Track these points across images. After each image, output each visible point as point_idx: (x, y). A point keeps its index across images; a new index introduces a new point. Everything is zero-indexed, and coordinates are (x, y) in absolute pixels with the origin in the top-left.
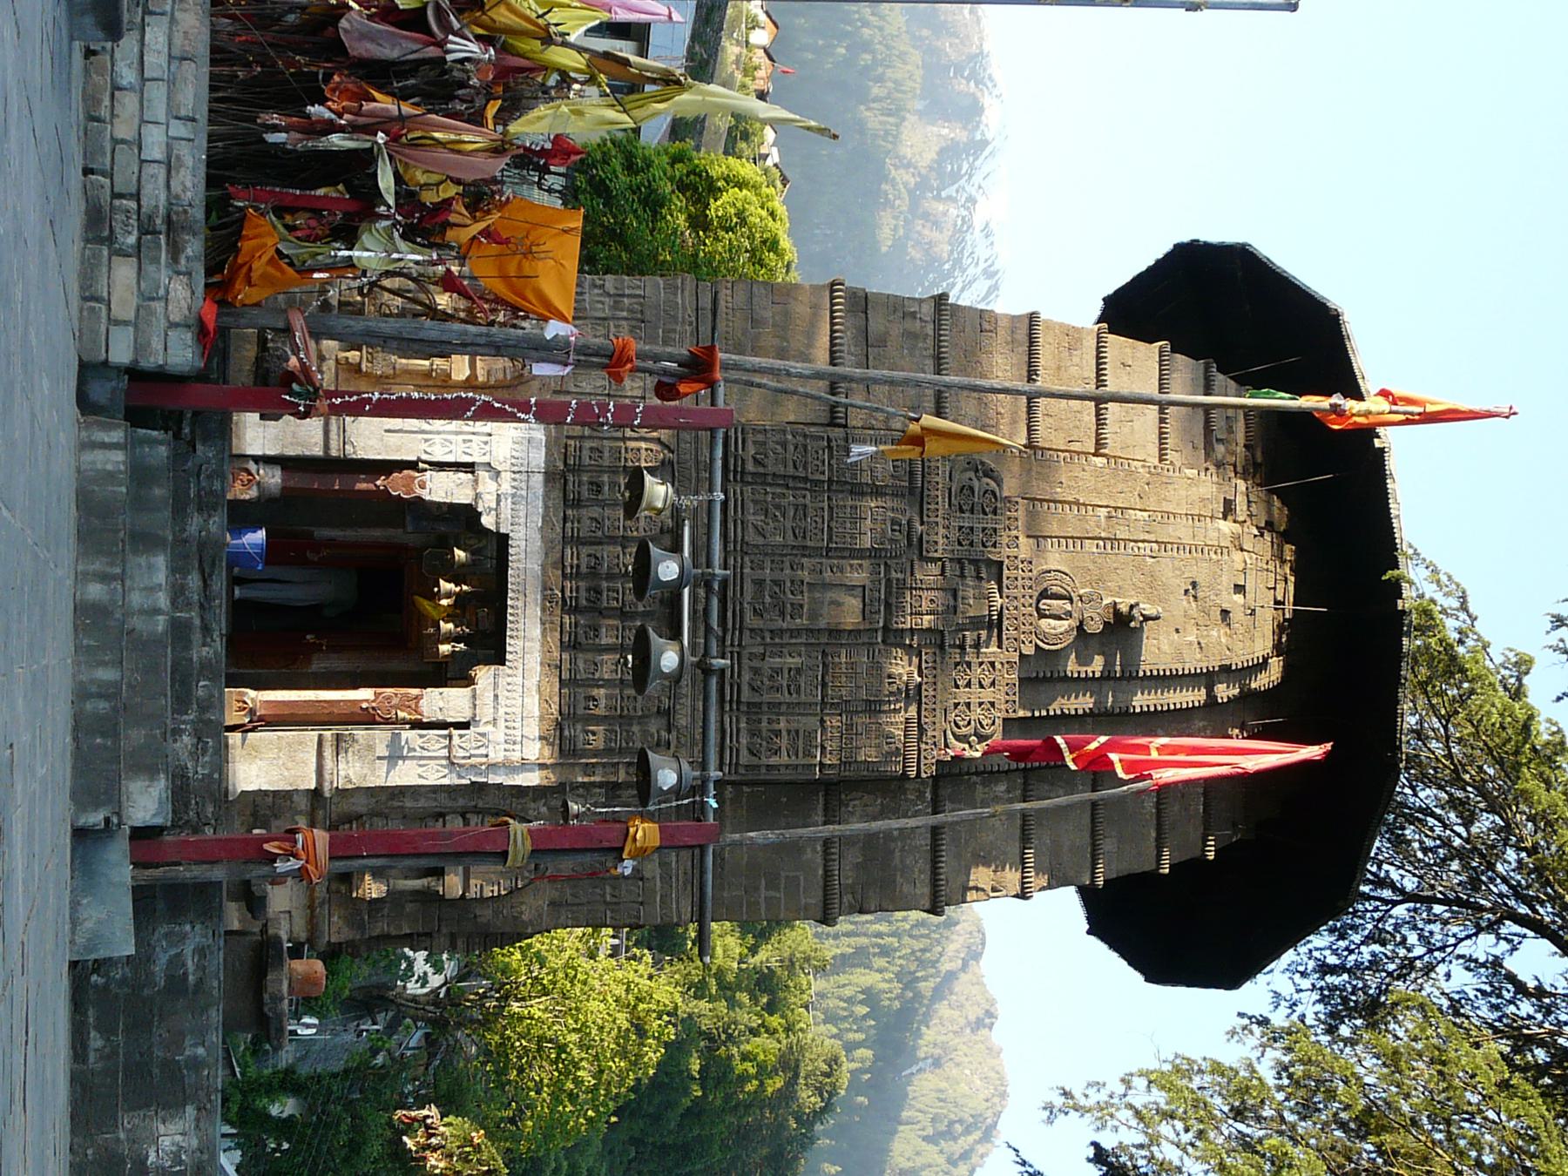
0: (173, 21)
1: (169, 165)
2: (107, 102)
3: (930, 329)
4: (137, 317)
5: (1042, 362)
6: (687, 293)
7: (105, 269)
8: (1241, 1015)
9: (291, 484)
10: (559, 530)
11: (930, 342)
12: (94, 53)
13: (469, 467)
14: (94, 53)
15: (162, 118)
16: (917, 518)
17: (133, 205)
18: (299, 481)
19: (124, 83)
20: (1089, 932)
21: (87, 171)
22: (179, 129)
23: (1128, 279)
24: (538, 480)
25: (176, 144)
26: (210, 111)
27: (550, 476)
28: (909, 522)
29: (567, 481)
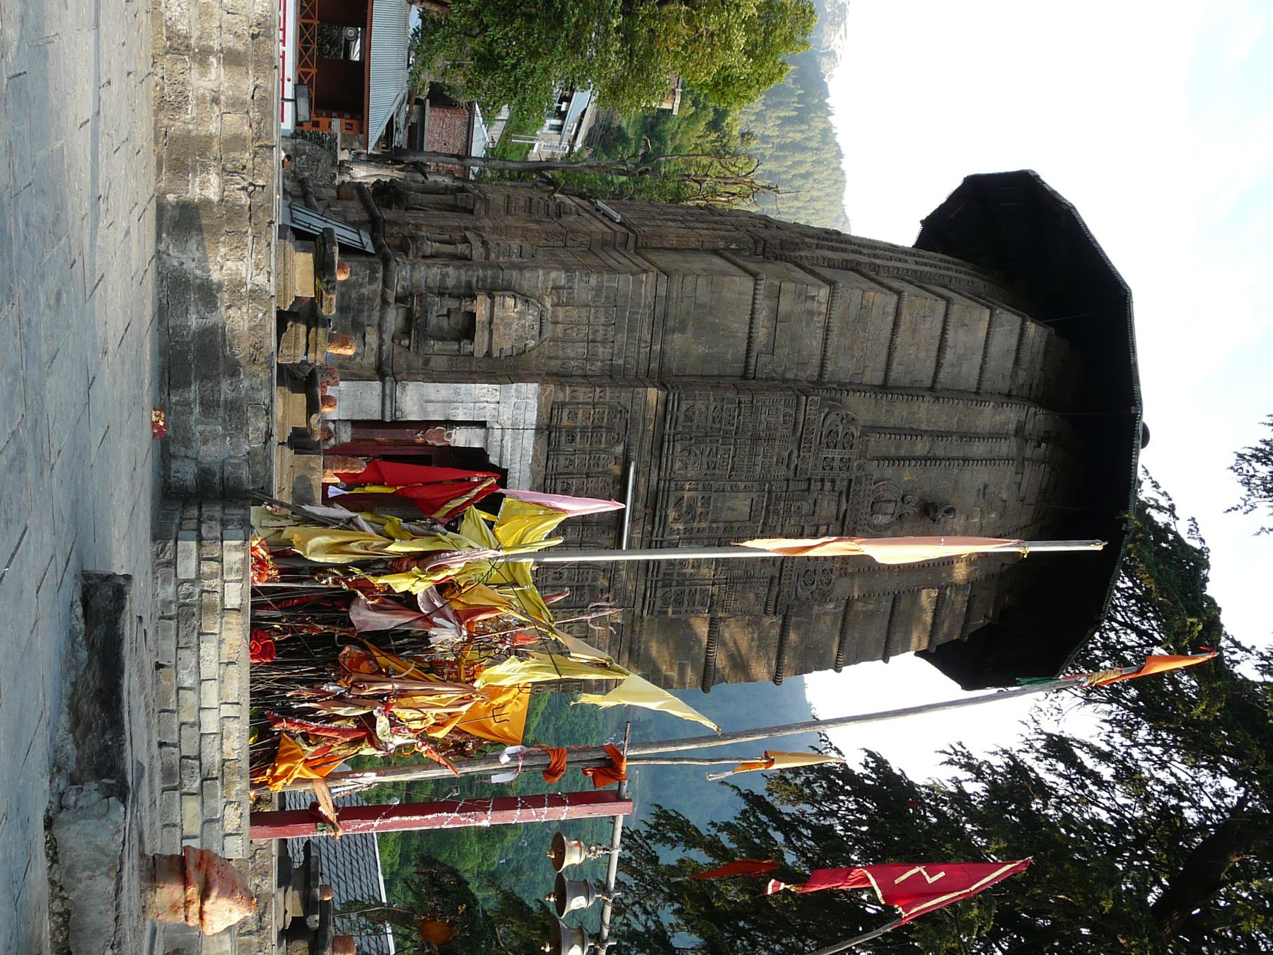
0: (221, 642)
1: (221, 735)
2: (173, 698)
3: (823, 309)
4: (202, 832)
5: (903, 327)
6: (649, 286)
7: (177, 805)
8: (960, 744)
9: (357, 436)
10: (543, 463)
11: (822, 317)
12: (162, 666)
13: (482, 424)
14: (162, 666)
15: (215, 704)
16: (795, 453)
17: (197, 763)
18: (363, 433)
19: (186, 685)
20: (922, 222)
21: (161, 745)
22: (227, 710)
23: (942, 199)
24: (530, 434)
25: (226, 722)
26: (252, 694)
27: (538, 430)
28: (790, 455)
29: (547, 430)
